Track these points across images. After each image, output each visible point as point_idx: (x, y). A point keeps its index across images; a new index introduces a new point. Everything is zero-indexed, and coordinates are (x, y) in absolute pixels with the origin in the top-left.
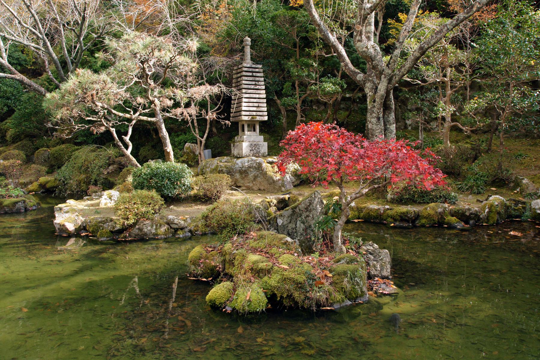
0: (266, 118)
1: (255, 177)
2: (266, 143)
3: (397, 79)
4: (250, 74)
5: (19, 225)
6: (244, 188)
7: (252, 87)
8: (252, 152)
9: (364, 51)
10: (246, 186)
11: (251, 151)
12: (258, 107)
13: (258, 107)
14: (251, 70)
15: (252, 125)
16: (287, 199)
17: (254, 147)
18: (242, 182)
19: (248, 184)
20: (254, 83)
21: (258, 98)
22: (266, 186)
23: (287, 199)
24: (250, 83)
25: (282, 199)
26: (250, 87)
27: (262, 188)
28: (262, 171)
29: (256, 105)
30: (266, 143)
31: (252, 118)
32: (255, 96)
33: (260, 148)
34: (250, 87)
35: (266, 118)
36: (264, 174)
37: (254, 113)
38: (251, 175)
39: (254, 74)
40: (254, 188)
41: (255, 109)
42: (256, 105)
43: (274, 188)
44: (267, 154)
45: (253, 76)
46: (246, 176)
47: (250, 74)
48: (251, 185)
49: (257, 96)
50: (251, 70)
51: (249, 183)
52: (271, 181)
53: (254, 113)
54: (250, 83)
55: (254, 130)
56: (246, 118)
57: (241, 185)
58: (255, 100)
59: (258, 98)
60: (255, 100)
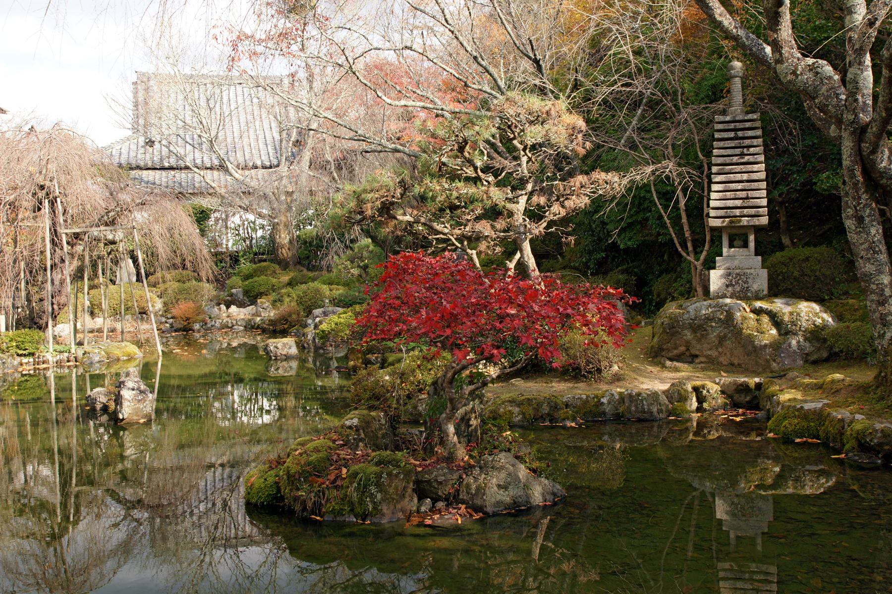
0: (764, 220)
1: (722, 340)
2: (765, 271)
3: (874, 129)
4: (732, 135)
5: (250, 370)
6: (703, 359)
7: (735, 159)
8: (730, 289)
9: (790, 82)
10: (707, 356)
11: (727, 286)
12: (747, 198)
13: (747, 198)
14: (732, 126)
15: (738, 237)
16: (752, 385)
17: (735, 278)
18: (698, 347)
19: (709, 353)
20: (738, 151)
21: (748, 181)
22: (742, 358)
23: (752, 385)
24: (729, 152)
25: (741, 385)
26: (728, 160)
27: (736, 362)
28: (735, 327)
29: (743, 194)
30: (765, 271)
31: (731, 222)
32: (738, 177)
33: (750, 281)
34: (728, 160)
35: (764, 220)
36: (737, 332)
37: (737, 212)
38: (713, 336)
39: (740, 134)
40: (721, 359)
41: (738, 203)
42: (743, 194)
43: (757, 363)
44: (766, 292)
45: (736, 138)
46: (702, 335)
47: (732, 135)
48: (714, 353)
49: (745, 177)
50: (732, 126)
51: (710, 349)
52: (750, 348)
53: (737, 212)
54: (729, 152)
55: (745, 245)
56: (716, 223)
57: (697, 353)
58: (739, 186)
59: (748, 181)
60: (739, 186)
